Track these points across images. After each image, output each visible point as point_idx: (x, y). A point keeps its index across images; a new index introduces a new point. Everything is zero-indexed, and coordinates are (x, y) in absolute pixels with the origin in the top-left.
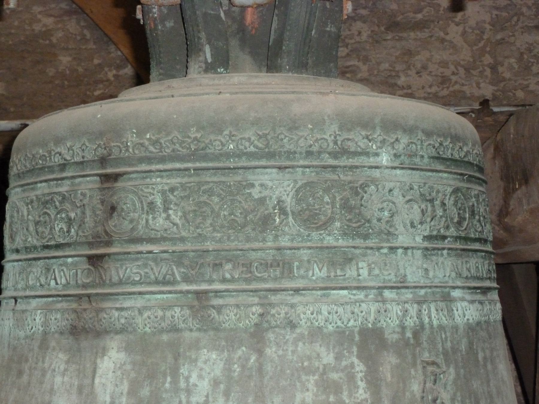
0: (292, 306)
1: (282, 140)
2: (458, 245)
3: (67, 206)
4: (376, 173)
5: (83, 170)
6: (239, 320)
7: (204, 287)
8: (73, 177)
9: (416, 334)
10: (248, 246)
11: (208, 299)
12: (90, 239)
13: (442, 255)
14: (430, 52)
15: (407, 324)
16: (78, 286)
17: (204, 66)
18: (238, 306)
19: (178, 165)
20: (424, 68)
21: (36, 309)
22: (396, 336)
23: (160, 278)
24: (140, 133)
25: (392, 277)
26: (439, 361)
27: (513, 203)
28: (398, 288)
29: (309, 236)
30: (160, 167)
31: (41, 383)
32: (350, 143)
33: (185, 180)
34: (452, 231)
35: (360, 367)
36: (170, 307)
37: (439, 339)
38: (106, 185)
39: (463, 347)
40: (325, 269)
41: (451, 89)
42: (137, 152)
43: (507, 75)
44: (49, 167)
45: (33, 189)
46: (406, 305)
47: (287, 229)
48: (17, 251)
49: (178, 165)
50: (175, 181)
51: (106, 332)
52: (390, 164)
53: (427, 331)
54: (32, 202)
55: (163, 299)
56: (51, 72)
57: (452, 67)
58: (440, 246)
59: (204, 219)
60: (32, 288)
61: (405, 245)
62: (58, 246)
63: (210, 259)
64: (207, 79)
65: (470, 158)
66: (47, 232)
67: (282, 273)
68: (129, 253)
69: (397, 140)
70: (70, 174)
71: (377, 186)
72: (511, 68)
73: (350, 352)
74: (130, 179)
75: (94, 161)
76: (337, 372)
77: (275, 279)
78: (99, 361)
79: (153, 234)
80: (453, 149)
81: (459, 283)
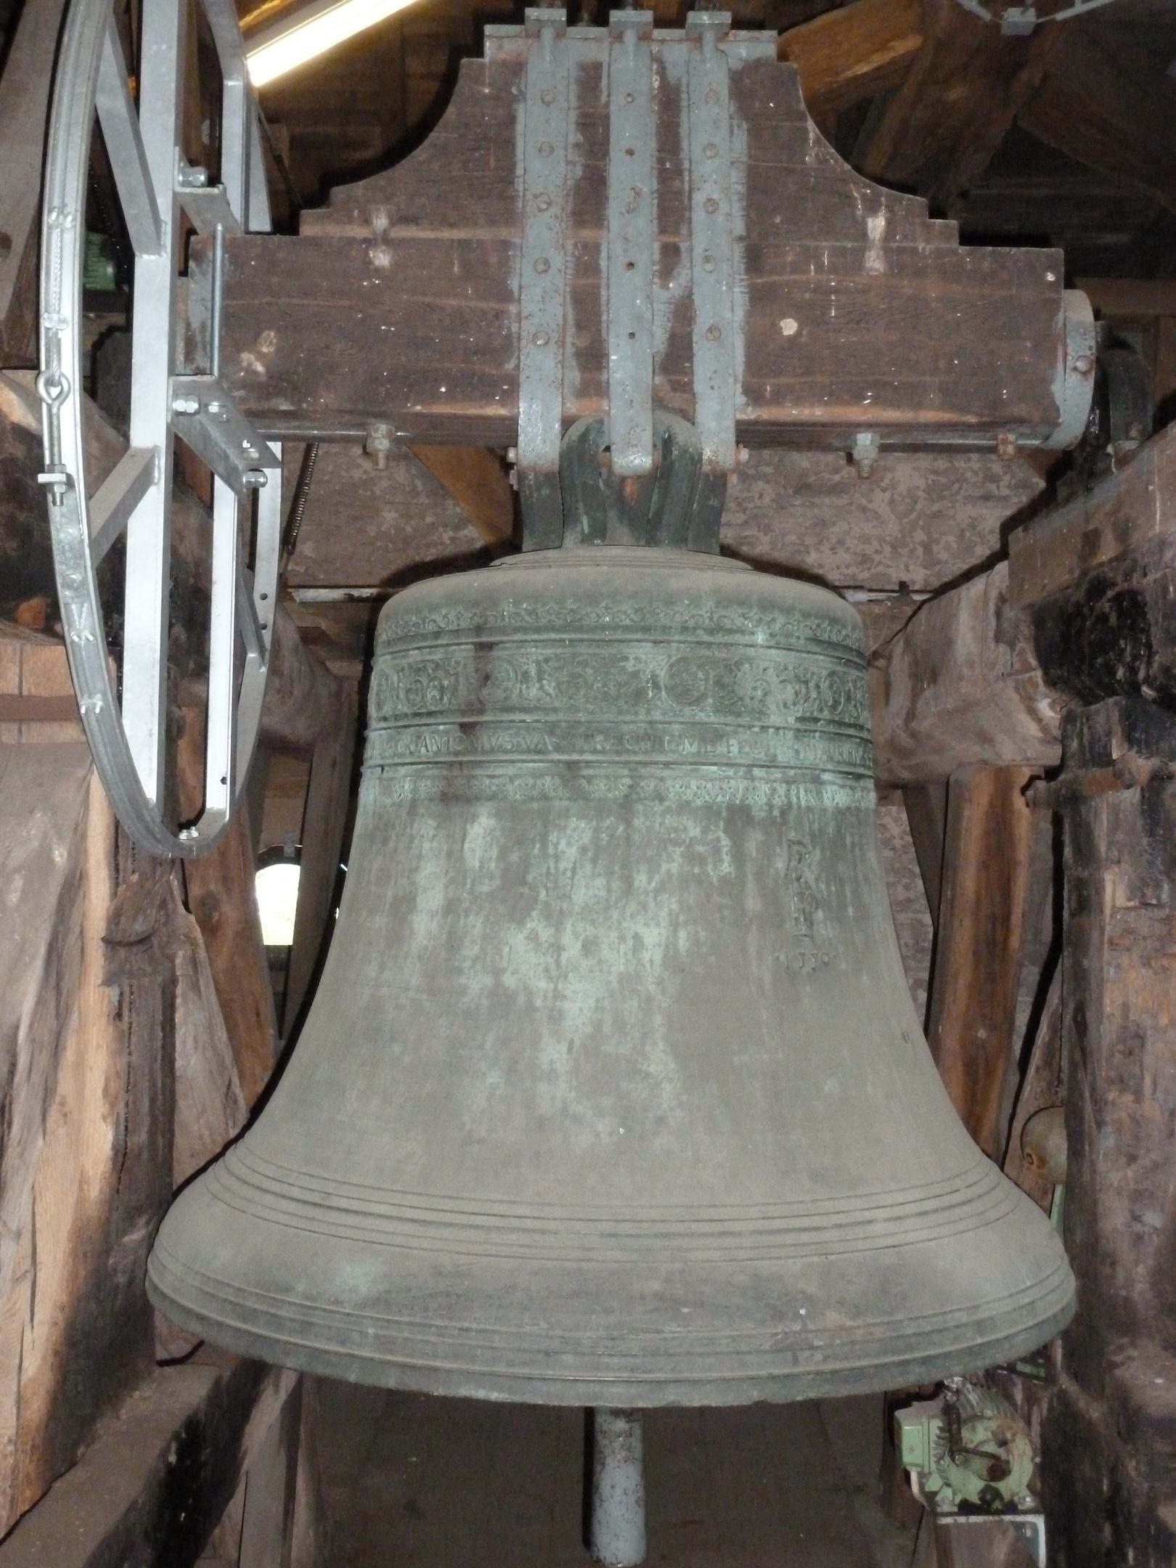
0: (662, 779)
1: (658, 614)
2: (831, 728)
3: (440, 673)
4: (751, 652)
5: (458, 638)
6: (609, 790)
7: (575, 757)
8: (448, 645)
9: (783, 813)
10: (620, 718)
11: (579, 769)
12: (463, 707)
13: (814, 737)
14: (849, 523)
15: (774, 802)
16: (449, 753)
17: (580, 537)
18: (607, 777)
19: (553, 636)
20: (841, 542)
21: (405, 776)
22: (763, 814)
23: (532, 747)
24: (517, 603)
25: (762, 756)
26: (805, 841)
27: (920, 705)
28: (768, 767)
29: (681, 711)
30: (536, 637)
31: (410, 848)
32: (726, 621)
33: (559, 651)
34: (826, 714)
35: (725, 842)
36: (542, 776)
37: (806, 820)
38: (481, 654)
39: (831, 830)
40: (696, 744)
41: (873, 571)
42: (513, 621)
43: (944, 556)
44: (422, 635)
45: (404, 657)
46: (775, 785)
47: (659, 703)
48: (385, 719)
49: (553, 636)
50: (549, 652)
51: (477, 799)
52: (766, 644)
53: (795, 812)
54: (403, 669)
55: (534, 769)
56: (372, 530)
57: (875, 543)
58: (813, 728)
59: (578, 689)
60: (402, 755)
61: (778, 725)
62: (430, 714)
63: (582, 729)
64: (585, 552)
65: (849, 642)
66: (419, 699)
67: (653, 747)
68: (502, 722)
69: (773, 619)
70: (444, 642)
71: (751, 665)
72: (948, 547)
73: (717, 826)
74: (505, 649)
75: (470, 629)
76: (703, 845)
77: (646, 752)
78: (468, 826)
79: (525, 704)
80: (831, 631)
81: (829, 767)
